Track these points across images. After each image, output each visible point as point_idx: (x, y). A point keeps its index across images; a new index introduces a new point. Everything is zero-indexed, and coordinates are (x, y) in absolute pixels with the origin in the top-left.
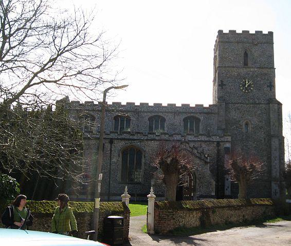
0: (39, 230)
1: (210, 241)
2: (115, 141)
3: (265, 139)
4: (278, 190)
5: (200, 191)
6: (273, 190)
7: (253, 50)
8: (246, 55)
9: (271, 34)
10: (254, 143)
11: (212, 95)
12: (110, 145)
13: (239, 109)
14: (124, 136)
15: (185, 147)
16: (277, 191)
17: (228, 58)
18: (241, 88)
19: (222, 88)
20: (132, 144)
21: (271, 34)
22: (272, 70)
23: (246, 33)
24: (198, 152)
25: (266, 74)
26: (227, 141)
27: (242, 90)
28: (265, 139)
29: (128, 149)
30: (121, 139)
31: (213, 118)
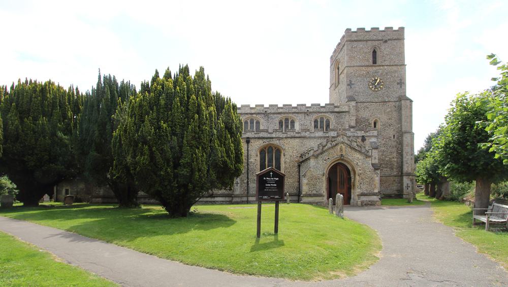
0: (404, 48)
1: (251, 218)
2: (252, 141)
3: (394, 136)
4: (410, 184)
5: (361, 188)
6: (405, 185)
7: (383, 48)
8: (374, 52)
9: (402, 30)
10: (383, 140)
11: (405, 45)
12: (247, 145)
13: (368, 108)
14: (261, 135)
15: (342, 140)
16: (409, 185)
17: (356, 57)
18: (371, 87)
19: (351, 88)
20: (271, 142)
21: (402, 30)
22: (402, 67)
23: (375, 29)
24: (357, 145)
25: (396, 71)
26: (372, 136)
27: (371, 89)
28: (394, 136)
29: (265, 148)
30: (259, 138)
31: (343, 116)
